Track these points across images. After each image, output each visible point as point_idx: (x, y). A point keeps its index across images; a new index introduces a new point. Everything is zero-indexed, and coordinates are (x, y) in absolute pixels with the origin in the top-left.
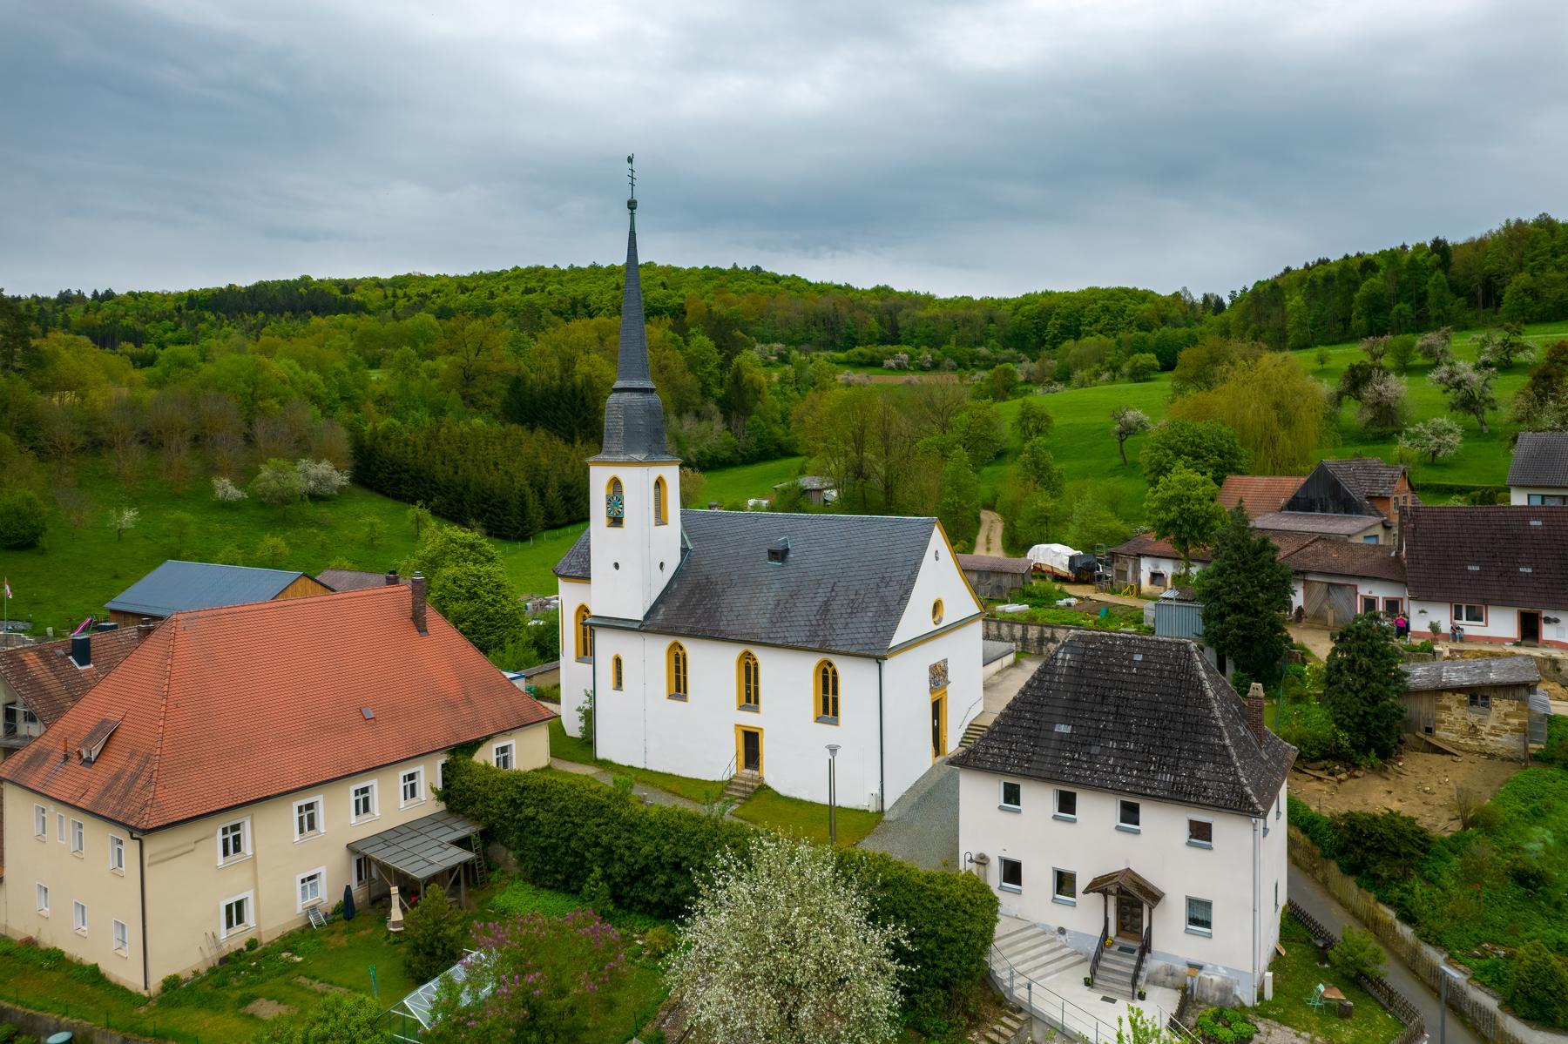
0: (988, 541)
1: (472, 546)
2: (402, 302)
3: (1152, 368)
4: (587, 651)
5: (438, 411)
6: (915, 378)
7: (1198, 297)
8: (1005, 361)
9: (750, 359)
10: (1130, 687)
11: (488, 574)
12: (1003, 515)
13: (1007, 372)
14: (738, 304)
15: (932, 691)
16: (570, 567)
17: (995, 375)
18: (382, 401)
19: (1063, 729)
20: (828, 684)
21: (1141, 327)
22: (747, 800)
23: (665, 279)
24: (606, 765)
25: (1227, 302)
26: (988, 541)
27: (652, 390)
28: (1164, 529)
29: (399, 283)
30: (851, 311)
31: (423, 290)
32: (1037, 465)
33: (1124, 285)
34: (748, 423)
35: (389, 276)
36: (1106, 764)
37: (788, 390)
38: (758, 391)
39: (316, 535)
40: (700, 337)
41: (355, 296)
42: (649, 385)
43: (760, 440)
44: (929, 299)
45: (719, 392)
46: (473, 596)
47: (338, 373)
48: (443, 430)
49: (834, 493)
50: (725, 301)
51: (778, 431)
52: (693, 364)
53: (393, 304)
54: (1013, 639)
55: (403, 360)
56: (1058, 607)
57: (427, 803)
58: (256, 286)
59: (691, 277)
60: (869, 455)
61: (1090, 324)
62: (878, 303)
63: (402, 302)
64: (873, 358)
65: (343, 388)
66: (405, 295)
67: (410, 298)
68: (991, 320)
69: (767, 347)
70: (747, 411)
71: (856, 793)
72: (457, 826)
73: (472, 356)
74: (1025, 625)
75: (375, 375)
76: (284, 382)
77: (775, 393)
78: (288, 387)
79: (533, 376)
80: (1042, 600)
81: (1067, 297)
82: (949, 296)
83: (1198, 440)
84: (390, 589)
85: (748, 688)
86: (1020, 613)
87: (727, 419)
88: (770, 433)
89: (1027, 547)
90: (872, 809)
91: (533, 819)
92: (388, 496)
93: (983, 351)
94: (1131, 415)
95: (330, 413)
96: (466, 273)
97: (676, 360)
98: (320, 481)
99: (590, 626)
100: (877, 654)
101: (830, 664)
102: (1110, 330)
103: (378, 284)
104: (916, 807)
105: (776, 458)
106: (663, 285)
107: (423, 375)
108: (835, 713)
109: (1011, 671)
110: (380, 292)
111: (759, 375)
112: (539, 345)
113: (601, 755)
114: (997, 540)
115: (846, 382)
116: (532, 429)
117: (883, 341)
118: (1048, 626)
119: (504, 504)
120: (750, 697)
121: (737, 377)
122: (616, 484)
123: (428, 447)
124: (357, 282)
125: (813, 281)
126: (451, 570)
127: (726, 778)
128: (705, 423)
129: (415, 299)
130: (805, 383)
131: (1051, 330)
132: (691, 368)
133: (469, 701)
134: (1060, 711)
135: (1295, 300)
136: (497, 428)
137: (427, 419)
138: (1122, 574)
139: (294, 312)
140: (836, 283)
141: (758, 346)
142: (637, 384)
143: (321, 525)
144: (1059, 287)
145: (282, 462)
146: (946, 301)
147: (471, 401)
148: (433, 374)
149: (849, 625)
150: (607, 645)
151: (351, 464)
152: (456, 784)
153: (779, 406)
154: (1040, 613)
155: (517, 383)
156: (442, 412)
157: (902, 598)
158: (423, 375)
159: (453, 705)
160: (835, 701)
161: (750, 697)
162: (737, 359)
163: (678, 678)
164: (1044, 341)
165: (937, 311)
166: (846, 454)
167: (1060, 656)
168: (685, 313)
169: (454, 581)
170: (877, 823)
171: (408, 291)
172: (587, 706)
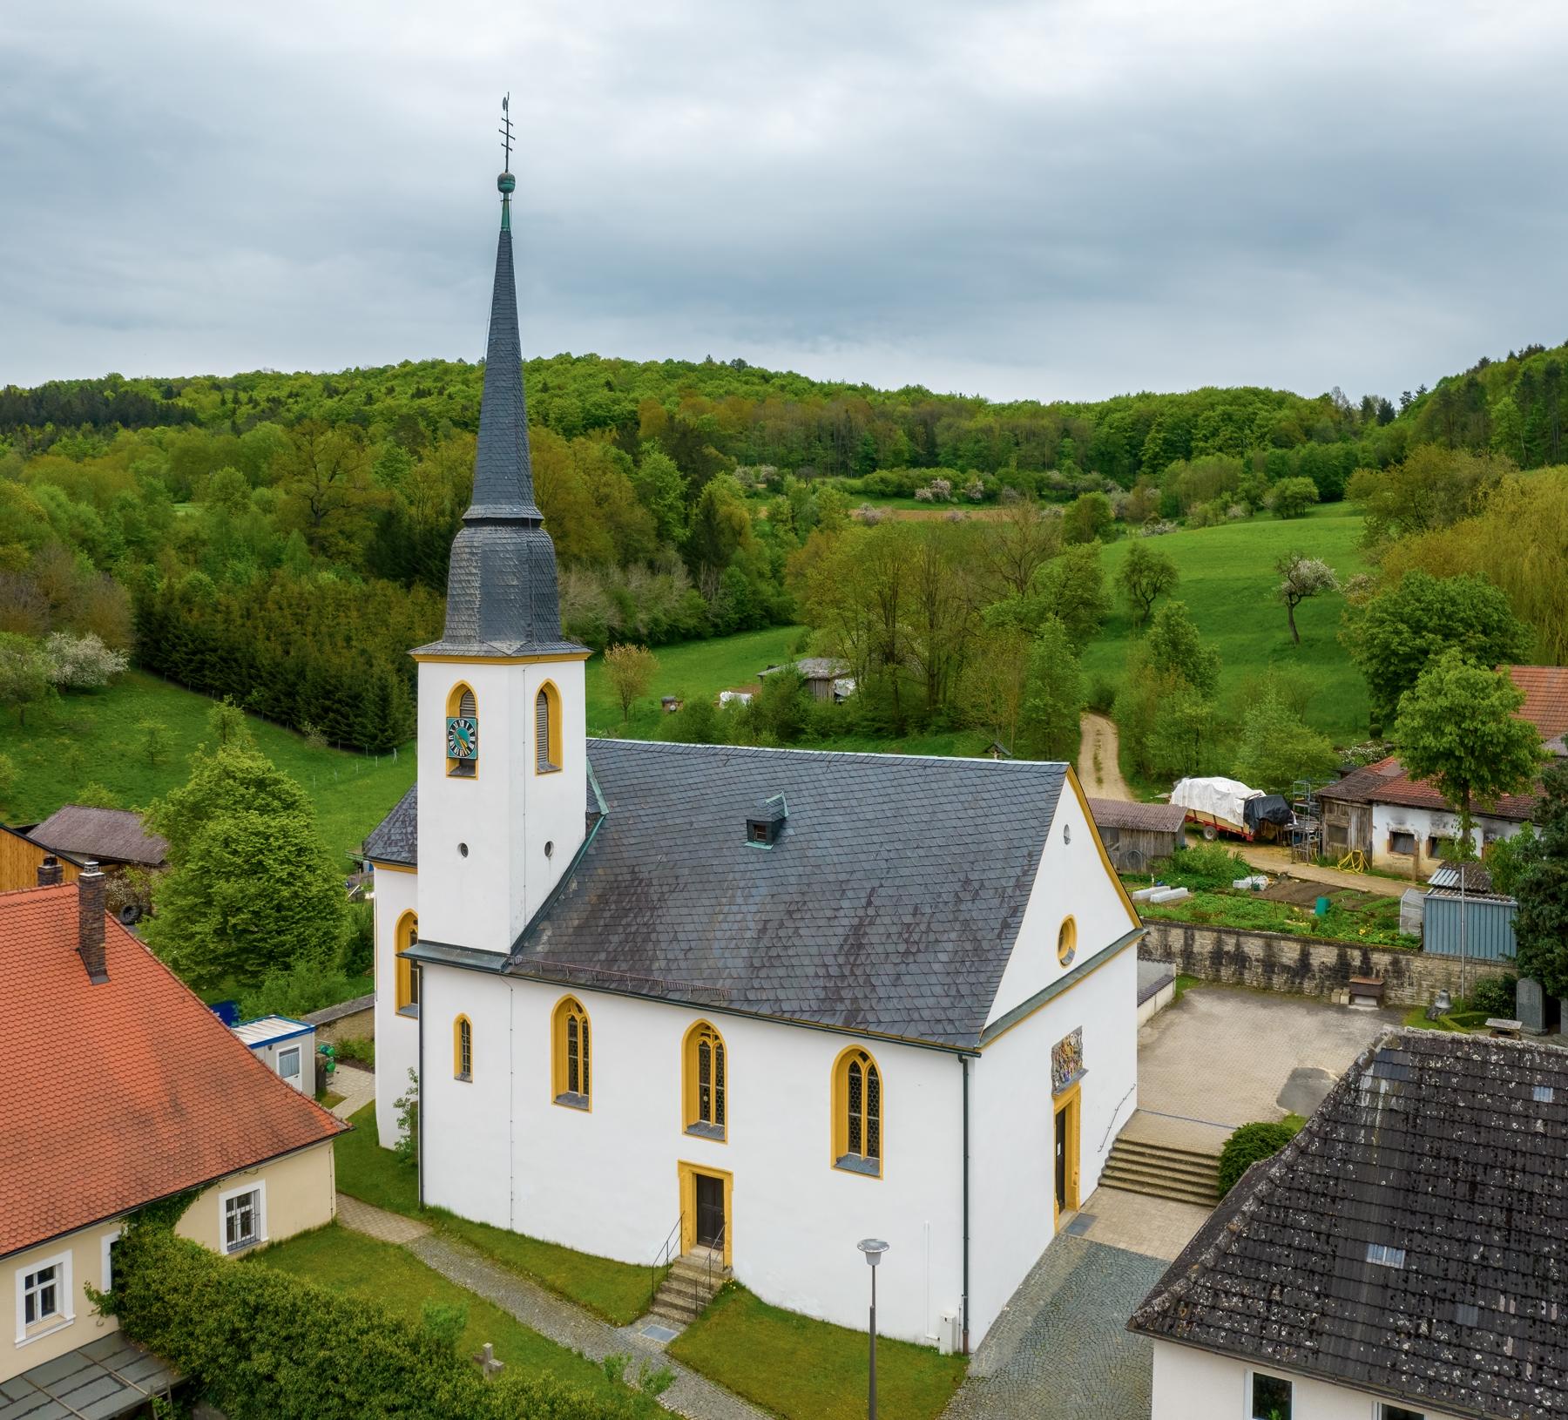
0: (1098, 766)
1: (261, 784)
2: (245, 409)
3: (1308, 499)
4: (412, 1000)
5: (272, 560)
6: (960, 513)
7: (1356, 402)
8: (1087, 490)
9: (728, 487)
10: (1534, 1164)
11: (284, 832)
12: (1118, 723)
13: (1097, 506)
14: (712, 412)
15: (1056, 1092)
16: (389, 842)
17: (1079, 509)
18: (189, 546)
19: (1385, 1257)
20: (860, 1095)
21: (1276, 443)
22: (700, 1314)
23: (611, 378)
24: (439, 1218)
25: (1397, 406)
26: (1098, 766)
27: (536, 523)
28: (1425, 763)
29: (243, 383)
30: (870, 421)
31: (275, 394)
32: (1175, 645)
33: (1251, 384)
34: (723, 577)
35: (230, 375)
36: (1495, 1353)
37: (781, 530)
38: (738, 532)
39: (67, 748)
40: (656, 455)
41: (182, 402)
42: (532, 512)
43: (740, 602)
44: (979, 405)
45: (681, 533)
46: (257, 869)
47: (125, 506)
48: (276, 589)
49: (851, 685)
50: (693, 406)
51: (767, 589)
52: (647, 493)
53: (234, 412)
54: (1168, 956)
55: (224, 487)
56: (1237, 893)
57: (77, 1322)
58: (45, 388)
59: (648, 375)
60: (904, 627)
61: (1206, 439)
62: (908, 409)
63: (245, 409)
64: (900, 485)
65: (131, 526)
66: (251, 400)
67: (256, 404)
68: (1066, 433)
69: (751, 471)
70: (721, 561)
71: (918, 1311)
72: (129, 1375)
73: (324, 481)
74: (1189, 929)
75: (181, 510)
76: (40, 518)
77: (763, 535)
78: (45, 527)
79: (413, 511)
80: (1210, 878)
81: (1173, 400)
82: (1007, 400)
83: (1449, 609)
84: (42, 894)
85: (705, 1091)
86: (1176, 903)
87: (693, 572)
88: (754, 593)
89: (1168, 780)
90: (946, 1348)
91: (270, 1378)
92: (185, 686)
93: (1055, 476)
94: (1306, 568)
95: (109, 563)
96: (336, 369)
97: (621, 487)
98: (82, 665)
99: (423, 957)
100: (959, 1039)
101: (864, 1056)
102: (1235, 446)
103: (215, 385)
104: (1032, 1340)
105: (763, 628)
106: (609, 385)
107: (253, 508)
108: (874, 1150)
109: (1172, 1016)
110: (215, 396)
111: (741, 510)
112: (427, 465)
113: (434, 1195)
114: (1111, 766)
115: (862, 519)
116: (408, 586)
117: (914, 463)
118: (1228, 932)
119: (356, 699)
120: (708, 1108)
121: (709, 512)
122: (464, 697)
123: (248, 614)
124: (186, 383)
125: (817, 380)
126: (223, 824)
127: (661, 1263)
128: (661, 578)
129: (264, 405)
130: (803, 521)
131: (1151, 446)
132: (643, 499)
133: (177, 1109)
134: (1375, 1214)
135: (1503, 404)
136: (357, 585)
137: (254, 572)
138: (1339, 832)
139: (95, 424)
140: (850, 382)
141: (740, 470)
142: (506, 510)
143: (76, 731)
144: (1163, 386)
145: (19, 638)
146: (1002, 408)
147: (320, 547)
148: (267, 507)
149: (903, 981)
150: (447, 995)
151: (131, 639)
152: (136, 1289)
153: (767, 553)
154: (1211, 903)
155: (389, 522)
156: (278, 562)
157: (1006, 925)
158: (253, 508)
159: (142, 1120)
160: (874, 1128)
161: (708, 1108)
162: (709, 487)
163: (573, 1064)
164: (1140, 463)
165: (990, 420)
166: (869, 627)
167: (1366, 1083)
168: (638, 423)
169: (226, 843)
170: (957, 1382)
171: (255, 394)
172: (415, 1098)
